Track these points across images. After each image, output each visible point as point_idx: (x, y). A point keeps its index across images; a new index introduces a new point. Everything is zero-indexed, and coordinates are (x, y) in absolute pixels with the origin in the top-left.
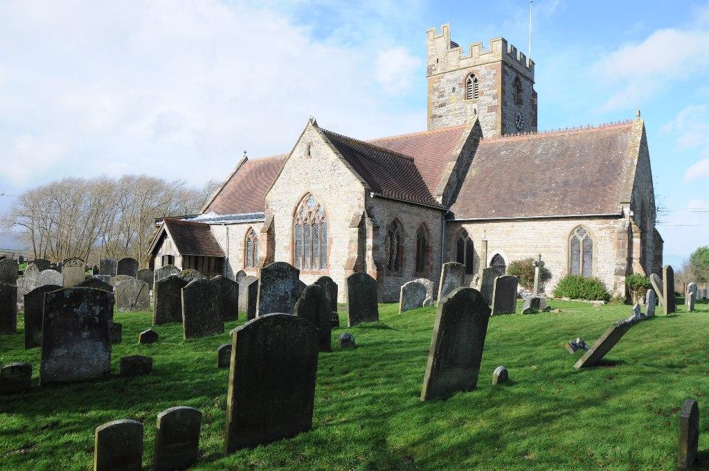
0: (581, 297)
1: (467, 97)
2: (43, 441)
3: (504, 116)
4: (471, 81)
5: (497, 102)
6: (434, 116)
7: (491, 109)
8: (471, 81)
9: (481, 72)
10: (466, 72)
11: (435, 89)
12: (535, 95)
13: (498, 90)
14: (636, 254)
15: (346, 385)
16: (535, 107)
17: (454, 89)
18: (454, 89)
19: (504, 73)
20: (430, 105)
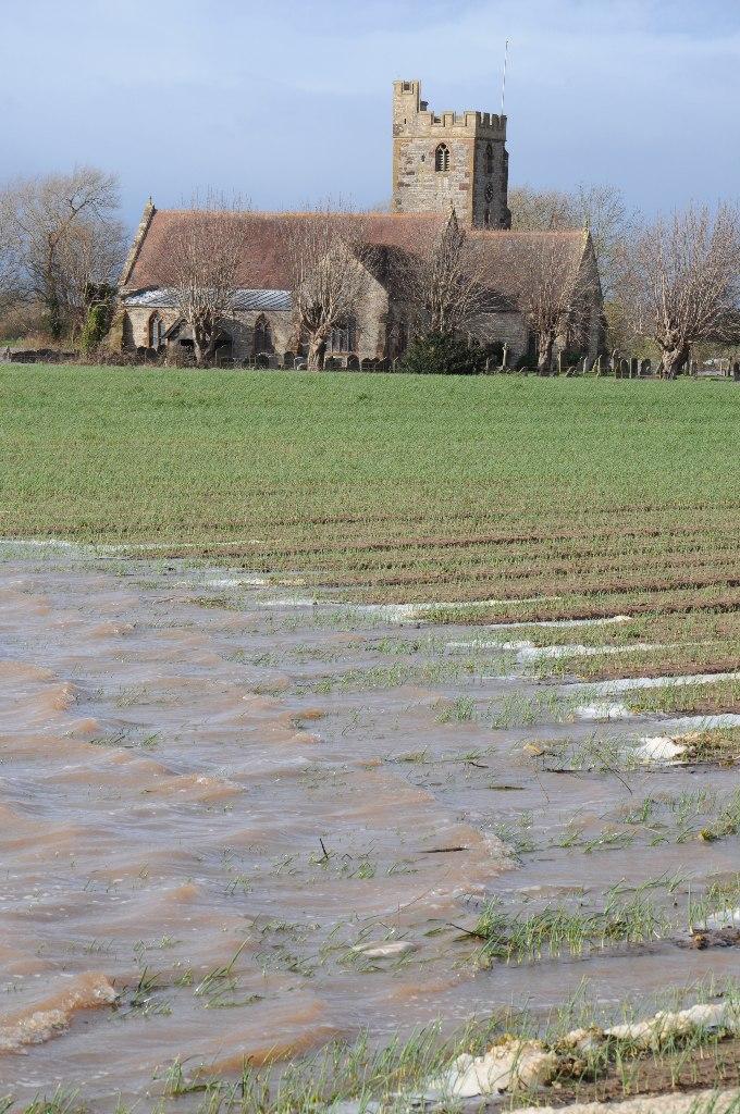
0: (641, 1093)
1: (438, 168)
2: (39, 655)
3: (475, 195)
4: (441, 154)
5: (468, 181)
6: (401, 184)
7: (463, 187)
8: (441, 154)
9: (453, 145)
10: (436, 142)
11: (403, 154)
12: (506, 155)
13: (470, 168)
14: (352, 811)
15: (664, 599)
16: (505, 170)
17: (423, 157)
18: (423, 157)
19: (477, 147)
20: (397, 169)
